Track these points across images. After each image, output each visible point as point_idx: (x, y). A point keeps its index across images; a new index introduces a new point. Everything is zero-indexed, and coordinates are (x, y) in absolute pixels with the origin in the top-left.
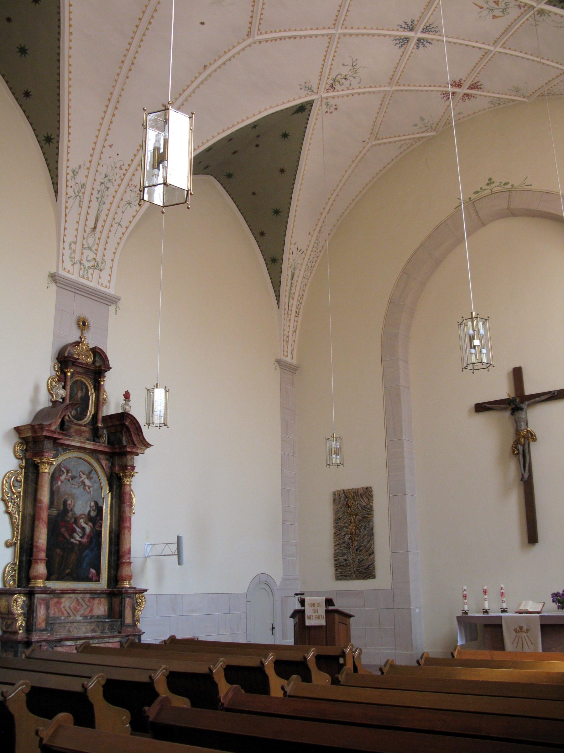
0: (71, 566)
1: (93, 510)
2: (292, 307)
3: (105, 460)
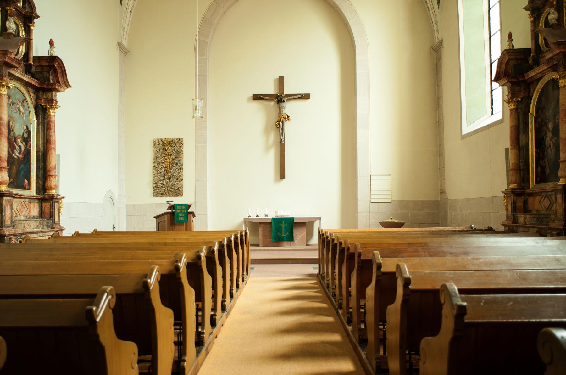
0: (13, 176)
2: (129, 6)
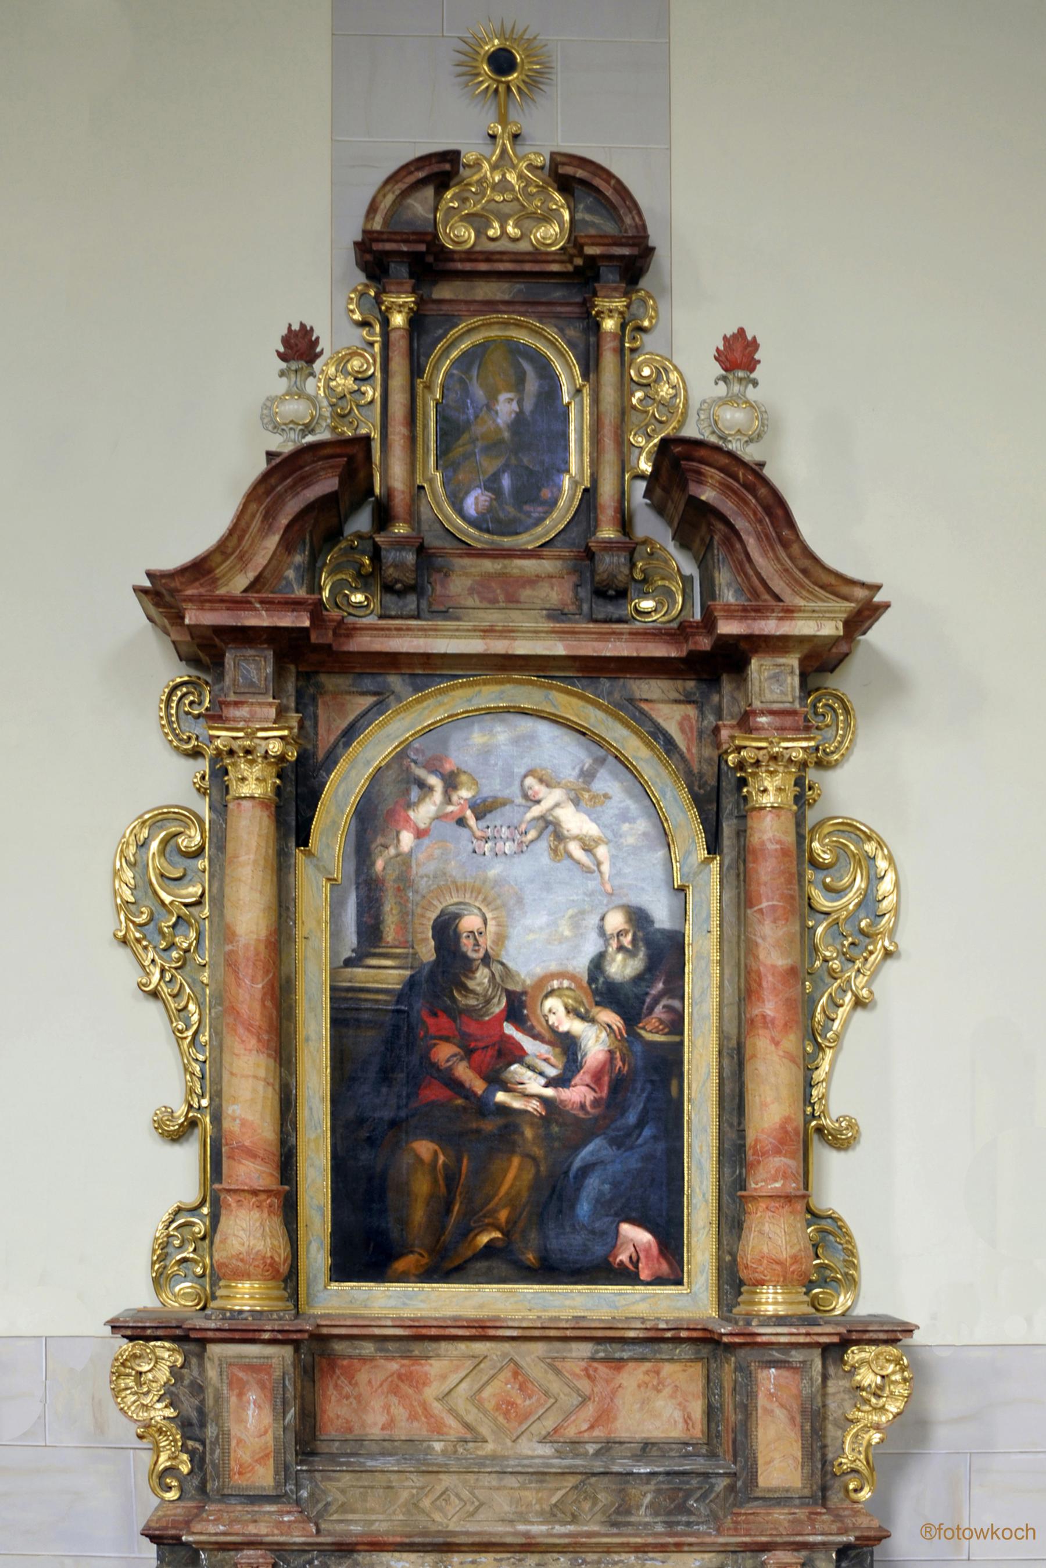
1: (621, 948)
3: (677, 702)
